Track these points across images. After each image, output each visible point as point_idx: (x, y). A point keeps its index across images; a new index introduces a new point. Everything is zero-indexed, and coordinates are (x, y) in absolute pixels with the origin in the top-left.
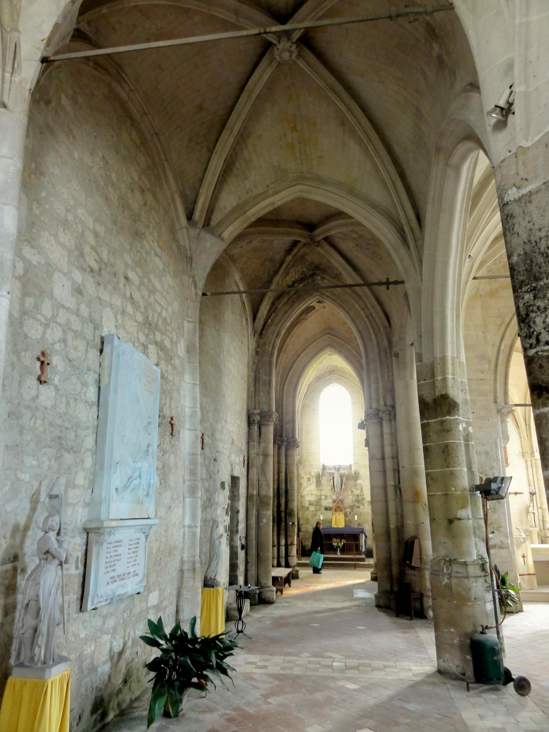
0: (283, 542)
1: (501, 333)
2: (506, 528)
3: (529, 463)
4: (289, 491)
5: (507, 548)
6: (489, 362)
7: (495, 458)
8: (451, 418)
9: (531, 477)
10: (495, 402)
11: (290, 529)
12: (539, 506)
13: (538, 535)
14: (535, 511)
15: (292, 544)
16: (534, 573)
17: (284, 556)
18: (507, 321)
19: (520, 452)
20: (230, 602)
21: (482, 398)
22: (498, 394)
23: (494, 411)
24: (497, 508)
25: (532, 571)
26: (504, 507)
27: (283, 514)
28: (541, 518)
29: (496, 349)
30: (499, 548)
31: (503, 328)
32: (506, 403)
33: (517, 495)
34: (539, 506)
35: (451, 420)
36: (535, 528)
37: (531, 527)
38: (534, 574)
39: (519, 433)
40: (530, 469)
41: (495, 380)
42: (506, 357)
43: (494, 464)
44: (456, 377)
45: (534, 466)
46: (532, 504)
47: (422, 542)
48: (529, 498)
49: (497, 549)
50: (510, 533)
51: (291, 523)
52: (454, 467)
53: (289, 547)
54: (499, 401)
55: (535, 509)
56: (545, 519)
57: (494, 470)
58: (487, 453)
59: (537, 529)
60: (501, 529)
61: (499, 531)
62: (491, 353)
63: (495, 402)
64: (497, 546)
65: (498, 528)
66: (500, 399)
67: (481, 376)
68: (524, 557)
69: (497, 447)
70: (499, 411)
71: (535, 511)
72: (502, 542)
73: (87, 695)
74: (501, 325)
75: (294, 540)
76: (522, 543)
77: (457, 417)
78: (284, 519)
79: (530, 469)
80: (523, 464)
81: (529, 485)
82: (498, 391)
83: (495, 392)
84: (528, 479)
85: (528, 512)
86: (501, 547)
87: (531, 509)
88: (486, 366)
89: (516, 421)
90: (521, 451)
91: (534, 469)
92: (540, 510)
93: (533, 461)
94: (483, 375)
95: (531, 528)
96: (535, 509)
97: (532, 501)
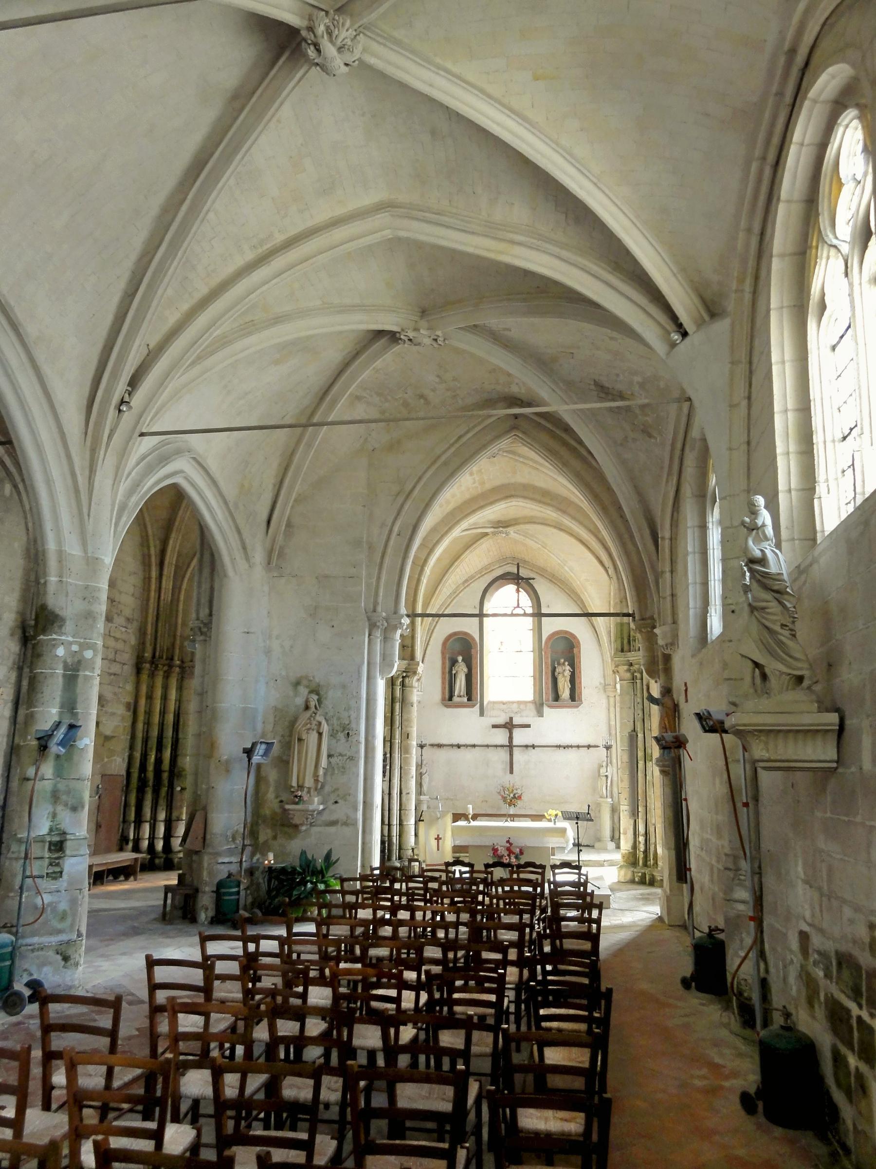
0: (162, 816)
3: (612, 700)
4: (180, 741)
7: (355, 694)
8: (45, 638)
9: (613, 723)
11: (177, 797)
15: (179, 819)
17: (161, 835)
18: (408, 487)
19: (601, 684)
20: (705, 918)
27: (165, 776)
30: (342, 825)
31: (401, 499)
35: (45, 640)
37: (601, 797)
44: (64, 579)
47: (209, 816)
49: (339, 826)
51: (179, 789)
52: (35, 707)
53: (174, 824)
57: (352, 713)
58: (344, 687)
61: (345, 800)
65: (344, 798)
68: (438, 839)
73: (314, 1062)
75: (181, 813)
77: (54, 636)
78: (166, 782)
79: (612, 709)
86: (345, 824)
90: (603, 682)
94: (355, 570)
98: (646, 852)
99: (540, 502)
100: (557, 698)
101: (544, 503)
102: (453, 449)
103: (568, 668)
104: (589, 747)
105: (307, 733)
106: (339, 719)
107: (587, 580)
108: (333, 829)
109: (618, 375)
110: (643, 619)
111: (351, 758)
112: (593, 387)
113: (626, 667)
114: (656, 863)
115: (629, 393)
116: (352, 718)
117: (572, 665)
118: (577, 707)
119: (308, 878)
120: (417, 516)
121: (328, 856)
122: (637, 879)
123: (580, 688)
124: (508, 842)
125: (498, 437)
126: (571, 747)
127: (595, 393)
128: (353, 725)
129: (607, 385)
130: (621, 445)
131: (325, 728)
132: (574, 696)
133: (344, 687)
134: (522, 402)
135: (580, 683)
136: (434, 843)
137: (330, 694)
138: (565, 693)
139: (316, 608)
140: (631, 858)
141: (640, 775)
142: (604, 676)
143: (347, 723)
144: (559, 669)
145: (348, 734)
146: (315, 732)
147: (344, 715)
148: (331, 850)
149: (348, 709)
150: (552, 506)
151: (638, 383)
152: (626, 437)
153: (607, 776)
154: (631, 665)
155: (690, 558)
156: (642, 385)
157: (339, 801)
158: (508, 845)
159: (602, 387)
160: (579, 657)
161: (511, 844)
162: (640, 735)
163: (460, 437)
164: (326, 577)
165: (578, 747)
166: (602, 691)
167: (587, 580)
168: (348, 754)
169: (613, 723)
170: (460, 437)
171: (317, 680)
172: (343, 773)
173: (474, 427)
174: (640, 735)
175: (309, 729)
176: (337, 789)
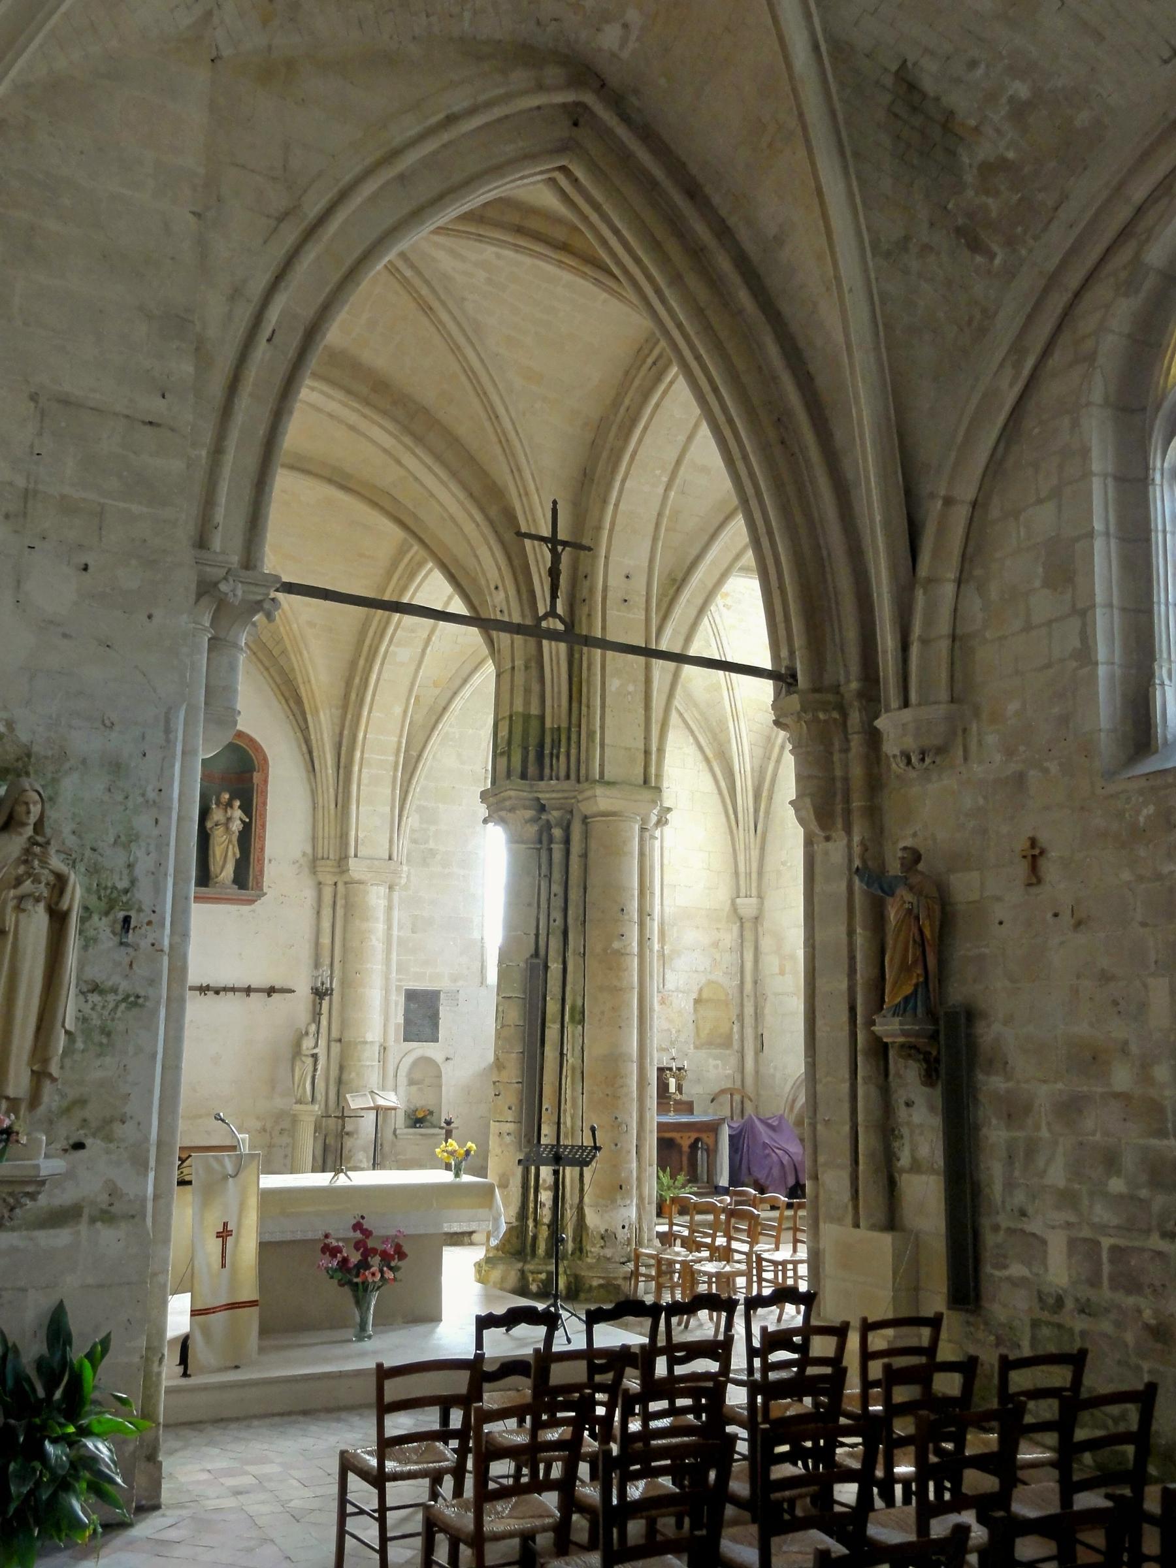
1: (278, 250)
2: (142, 1125)
3: (328, 893)
5: (135, 1216)
6: (201, 353)
7: (151, 795)
9: (326, 940)
10: (202, 543)
12: (335, 1034)
13: (317, 1129)
14: (321, 1051)
16: (254, 1296)
19: (304, 854)
21: (135, 508)
22: (220, 515)
23: (186, 579)
24: (121, 1027)
25: (248, 1293)
26: (151, 1028)
28: (334, 1073)
29: (244, 314)
30: (93, 1221)
31: (290, 235)
32: (250, 561)
33: (275, 995)
34: (335, 1034)
36: (310, 1107)
37: (299, 1102)
38: (253, 1303)
39: (313, 793)
40: (327, 912)
41: (218, 451)
42: (283, 369)
43: (142, 823)
45: (340, 903)
46: (313, 1028)
48: (310, 1007)
49: (83, 1227)
50: (160, 1144)
54: (217, 544)
55: (322, 1042)
56: (345, 1077)
57: (138, 852)
59: (316, 1108)
60: (119, 1130)
61: (109, 1139)
62: (220, 321)
63: (202, 543)
64: (86, 1212)
65: (105, 1129)
66: (226, 542)
67: (154, 406)
68: (224, 1234)
69: (169, 742)
70: (206, 589)
71: (321, 1051)
72: (113, 1192)
74: (283, 217)
76: (226, 1177)
79: (327, 912)
80: (309, 894)
81: (317, 965)
82: (222, 499)
83: (209, 502)
84: (317, 944)
85: (297, 1052)
86: (106, 1217)
87: (308, 1043)
88: (186, 368)
89: (310, 752)
90: (309, 851)
91: (340, 912)
92: (336, 1048)
93: (340, 886)
94: (162, 403)
95: (298, 1107)
96: (322, 1042)
97: (316, 1015)
98: (556, 1226)
99: (367, 402)
100: (204, 877)
101: (374, 407)
102: (430, 146)
103: (238, 813)
104: (271, 991)
105: (19, 908)
106: (94, 870)
107: (311, 624)
108: (61, 1237)
109: (973, 64)
110: (816, 690)
111: (134, 1001)
112: (888, 81)
113: (530, 813)
114: (580, 1249)
115: (972, 123)
116: (139, 871)
117: (247, 808)
118: (251, 902)
119: (787, 1517)
120: (321, 299)
121: (57, 1330)
122: (534, 1288)
123: (261, 860)
124: (357, 1226)
125: (529, 157)
126: (233, 990)
127: (886, 98)
128: (143, 894)
129: (928, 85)
130: (888, 254)
131: (76, 896)
132: (246, 877)
133: (116, 767)
134: (603, 86)
135: (262, 849)
136: (214, 1245)
137: (69, 785)
138: (227, 873)
139: (27, 495)
140: (514, 1240)
141: (550, 1053)
142: (314, 838)
143: (122, 884)
144: (217, 815)
145: (127, 920)
146: (41, 908)
147: (115, 859)
148: (61, 1303)
149: (127, 840)
150: (395, 420)
151: (1011, 99)
152: (907, 239)
153: (315, 1057)
154: (542, 808)
155: (1099, 544)
156: (1019, 112)
157: (88, 1142)
158: (358, 1235)
159: (912, 87)
160: (264, 793)
161: (367, 1233)
162: (555, 967)
163: (451, 120)
164: (65, 401)
165: (248, 990)
166: (306, 871)
167: (311, 624)
168: (124, 986)
169: (326, 940)
170: (451, 120)
171: (24, 737)
172: (102, 1051)
173: (489, 104)
174: (555, 967)
175: (21, 898)
176: (81, 1102)
